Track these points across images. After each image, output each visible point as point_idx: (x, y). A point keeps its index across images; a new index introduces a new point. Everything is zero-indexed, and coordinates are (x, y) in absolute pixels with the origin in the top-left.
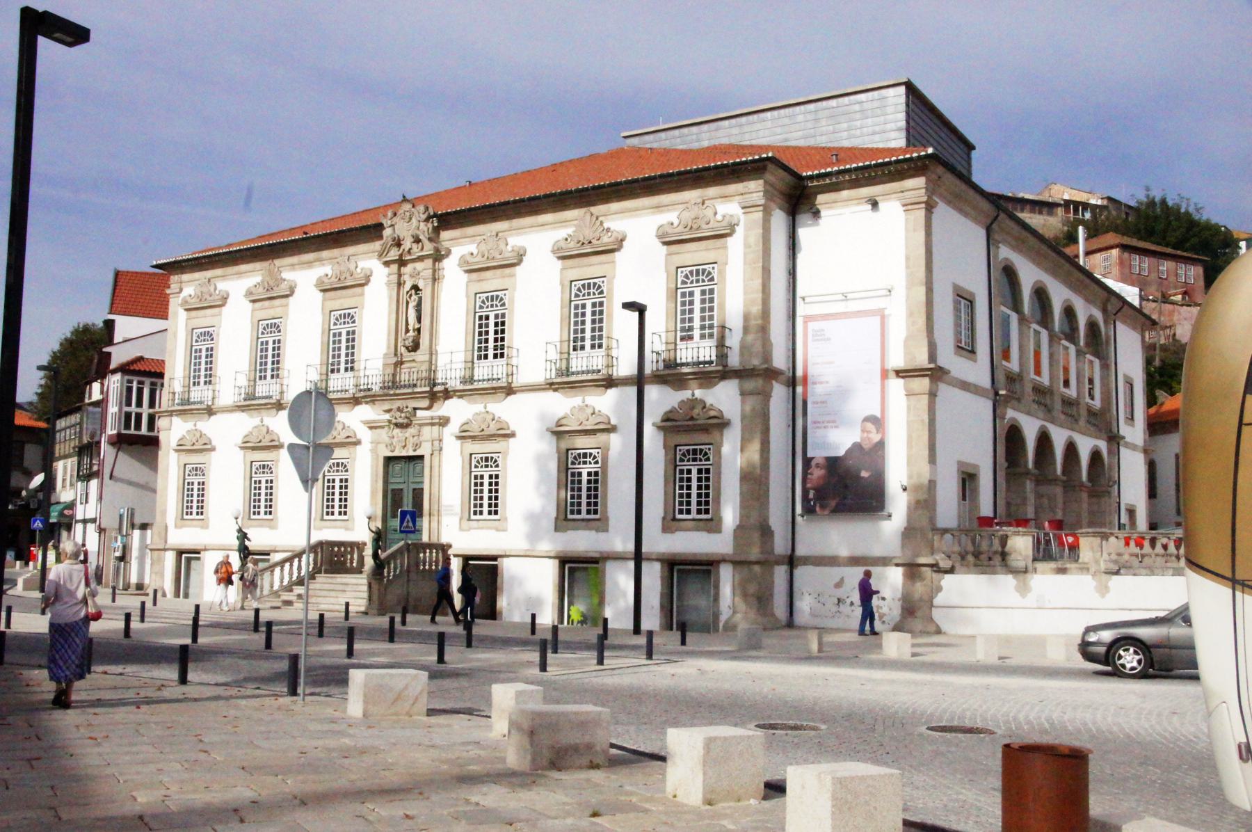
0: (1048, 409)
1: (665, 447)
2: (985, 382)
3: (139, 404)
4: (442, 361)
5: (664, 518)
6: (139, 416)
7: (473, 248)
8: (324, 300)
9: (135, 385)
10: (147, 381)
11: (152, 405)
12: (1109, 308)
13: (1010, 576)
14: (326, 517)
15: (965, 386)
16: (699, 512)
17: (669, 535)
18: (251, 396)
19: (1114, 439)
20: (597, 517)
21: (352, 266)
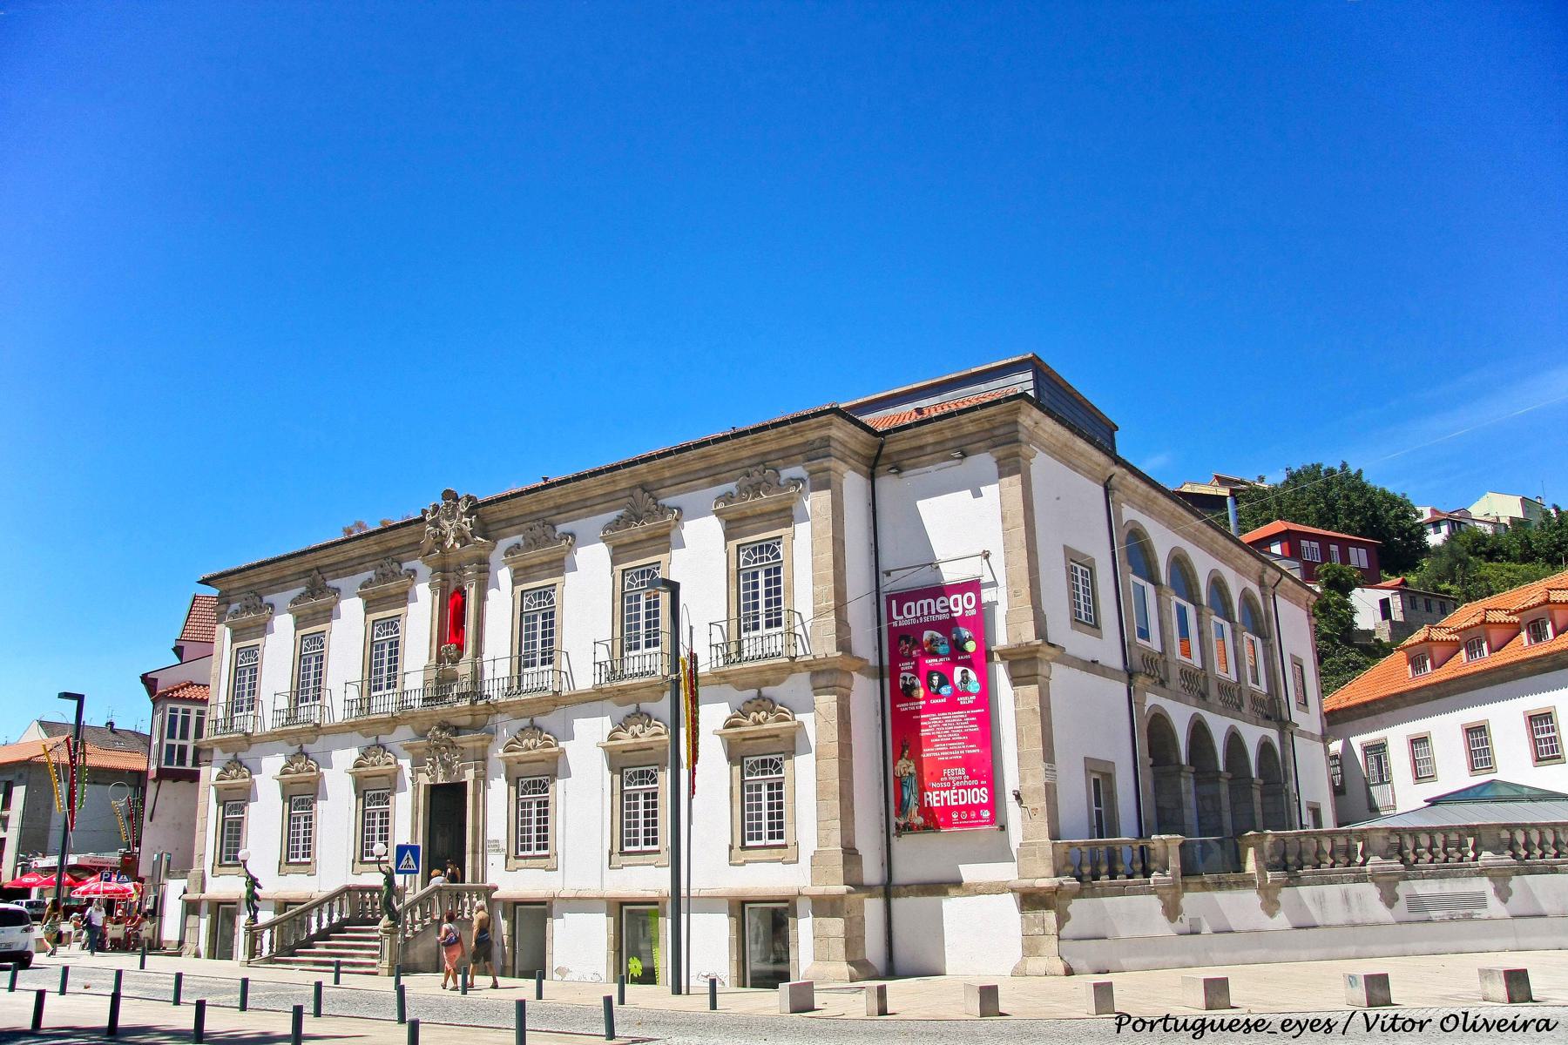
0: (1203, 695)
2: (1117, 663)
3: (184, 736)
6: (183, 750)
9: (180, 715)
10: (194, 709)
11: (199, 734)
12: (1266, 578)
14: (748, 843)
15: (1092, 666)
16: (771, 836)
19: (1285, 726)
20: (655, 848)
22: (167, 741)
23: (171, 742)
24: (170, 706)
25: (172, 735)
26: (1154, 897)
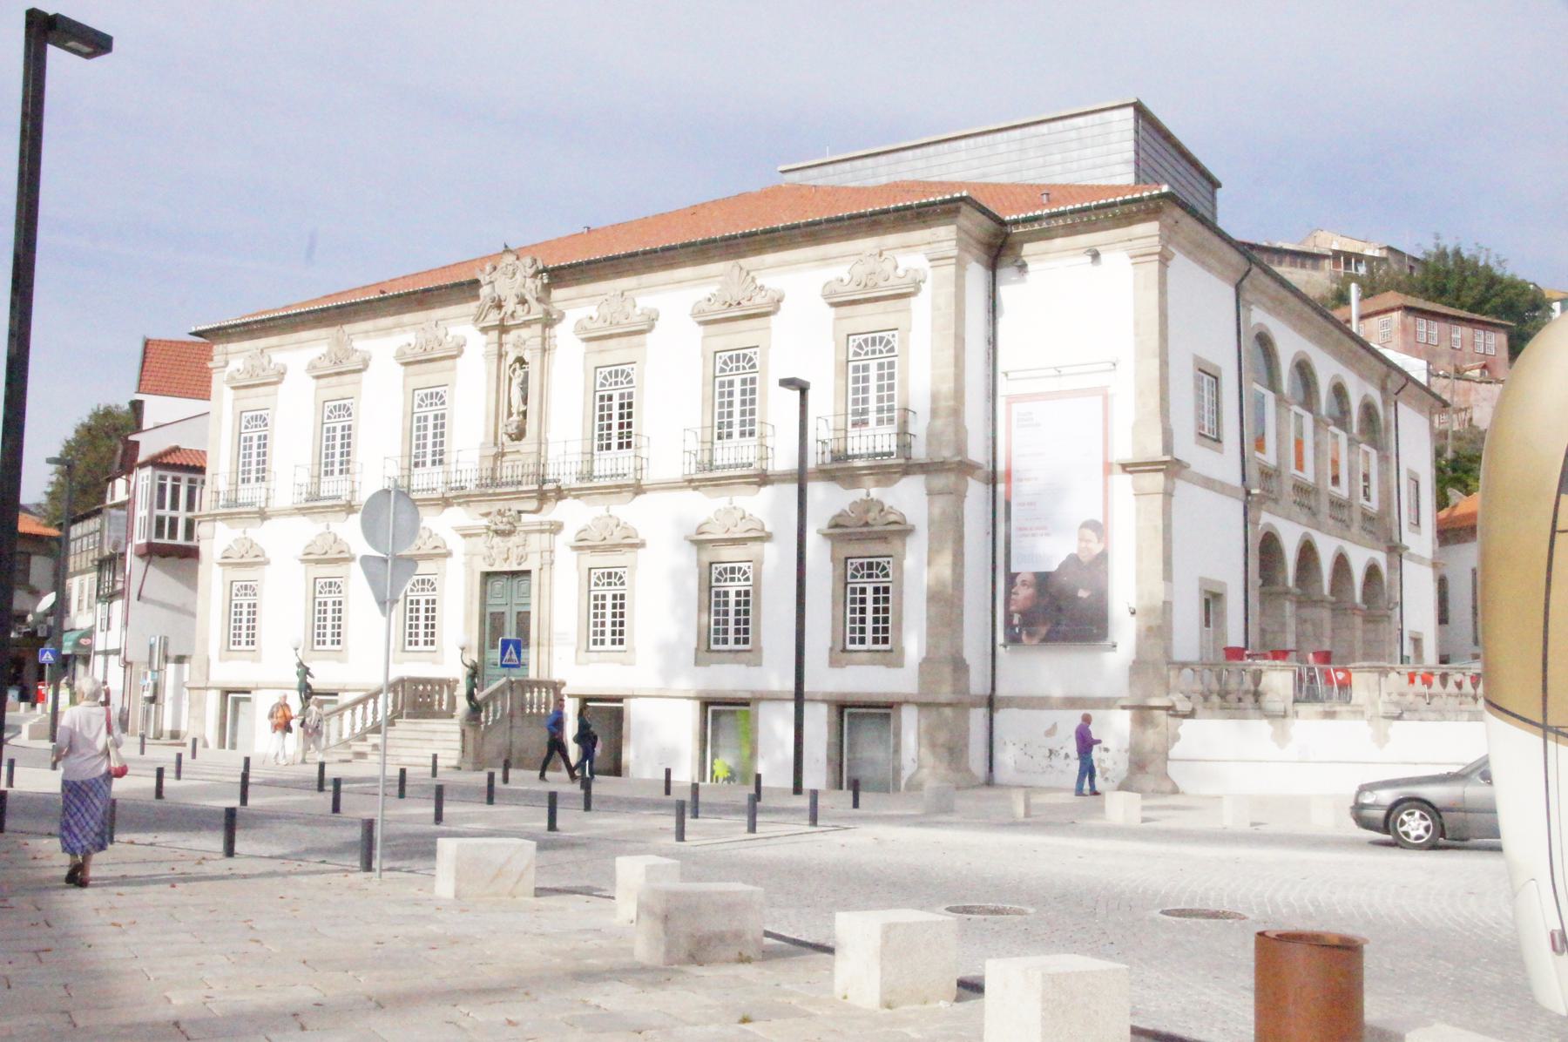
0: (1313, 512)
1: (833, 559)
2: (1235, 479)
3: (175, 506)
4: (553, 453)
5: (831, 649)
6: (174, 521)
7: (592, 311)
9: (169, 483)
10: (185, 477)
11: (190, 506)
12: (1389, 385)
15: (1209, 483)
16: (876, 641)
17: (837, 671)
18: (314, 497)
19: (1395, 550)
21: (441, 334)
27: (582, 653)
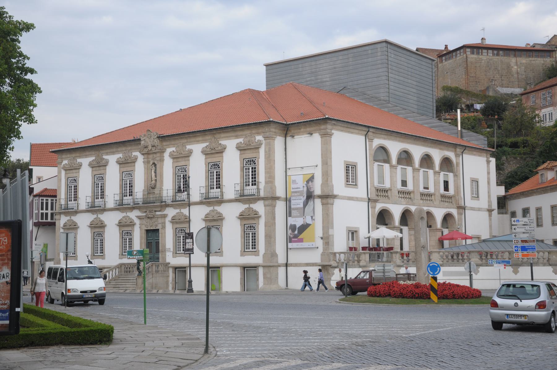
1: (241, 225)
3: (47, 209)
4: (164, 194)
6: (47, 214)
7: (174, 149)
8: (92, 171)
9: (45, 201)
10: (50, 199)
11: (52, 209)
13: (550, 267)
16: (252, 248)
17: (243, 257)
18: (93, 206)
21: (130, 155)
22: (41, 211)
23: (42, 211)
24: (41, 198)
25: (42, 209)
26: (29, 159)
27: (174, 254)
